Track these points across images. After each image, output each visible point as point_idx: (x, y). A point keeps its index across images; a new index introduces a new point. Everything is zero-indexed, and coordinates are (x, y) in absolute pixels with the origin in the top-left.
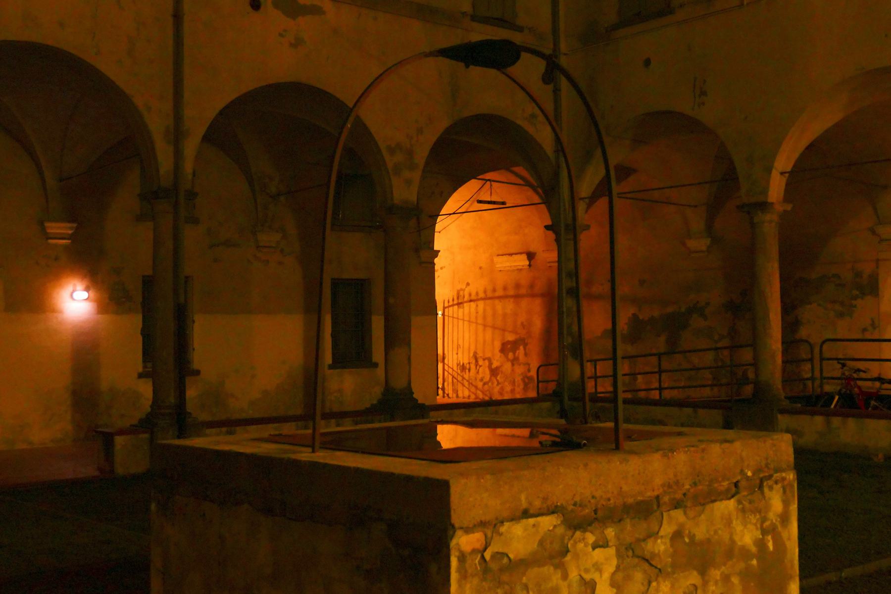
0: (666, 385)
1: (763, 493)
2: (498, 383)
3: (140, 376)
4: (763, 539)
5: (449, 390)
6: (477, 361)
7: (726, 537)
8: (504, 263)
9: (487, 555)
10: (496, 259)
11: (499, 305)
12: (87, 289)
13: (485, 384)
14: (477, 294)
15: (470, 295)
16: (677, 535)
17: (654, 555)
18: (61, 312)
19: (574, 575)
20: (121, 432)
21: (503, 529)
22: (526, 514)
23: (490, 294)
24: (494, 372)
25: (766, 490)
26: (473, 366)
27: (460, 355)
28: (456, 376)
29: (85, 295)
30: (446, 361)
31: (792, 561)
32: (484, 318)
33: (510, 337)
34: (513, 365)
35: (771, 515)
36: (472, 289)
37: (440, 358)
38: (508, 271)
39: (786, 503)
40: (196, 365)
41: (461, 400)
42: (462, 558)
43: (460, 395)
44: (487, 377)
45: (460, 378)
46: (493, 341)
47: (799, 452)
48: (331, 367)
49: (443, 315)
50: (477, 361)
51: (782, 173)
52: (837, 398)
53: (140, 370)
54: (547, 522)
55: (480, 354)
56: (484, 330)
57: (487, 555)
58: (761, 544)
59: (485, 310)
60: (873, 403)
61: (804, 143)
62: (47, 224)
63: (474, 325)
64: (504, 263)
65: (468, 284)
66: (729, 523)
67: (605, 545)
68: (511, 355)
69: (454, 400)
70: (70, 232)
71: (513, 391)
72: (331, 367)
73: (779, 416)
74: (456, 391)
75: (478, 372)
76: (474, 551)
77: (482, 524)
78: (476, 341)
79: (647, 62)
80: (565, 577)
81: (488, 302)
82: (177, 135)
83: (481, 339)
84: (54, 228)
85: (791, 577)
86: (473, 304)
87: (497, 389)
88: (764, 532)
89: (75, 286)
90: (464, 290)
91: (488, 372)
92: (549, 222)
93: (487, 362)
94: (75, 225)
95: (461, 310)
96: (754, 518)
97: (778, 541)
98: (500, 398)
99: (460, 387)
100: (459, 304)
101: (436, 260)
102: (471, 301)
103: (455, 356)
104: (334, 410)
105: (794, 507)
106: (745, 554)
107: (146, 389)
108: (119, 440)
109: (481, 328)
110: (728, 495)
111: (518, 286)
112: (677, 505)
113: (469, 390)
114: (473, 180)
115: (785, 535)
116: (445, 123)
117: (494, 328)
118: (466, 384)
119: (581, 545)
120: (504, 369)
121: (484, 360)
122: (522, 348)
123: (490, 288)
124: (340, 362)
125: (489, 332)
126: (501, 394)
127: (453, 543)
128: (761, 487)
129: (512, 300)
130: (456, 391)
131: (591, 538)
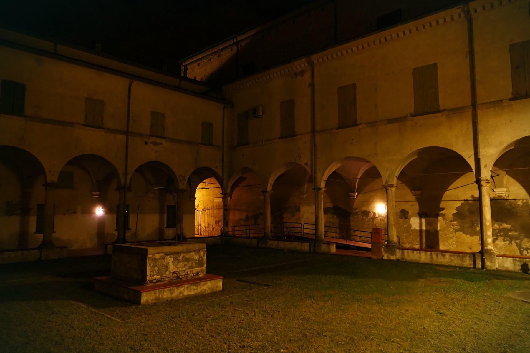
0: (251, 233)
1: (199, 252)
2: (214, 232)
3: (115, 230)
4: (199, 258)
5: (202, 233)
6: (209, 225)
7: (192, 257)
8: (216, 200)
9: (153, 258)
10: (214, 199)
11: (215, 211)
12: (103, 208)
13: (211, 232)
14: (210, 208)
15: (208, 208)
16: (183, 257)
17: (179, 259)
18: (96, 214)
19: (166, 261)
20: (109, 244)
21: (155, 255)
22: (159, 253)
23: (212, 208)
24: (213, 229)
25: (200, 252)
26: (208, 227)
27: (205, 224)
28: (204, 229)
29: (102, 210)
30: (201, 225)
31: (205, 262)
32: (211, 214)
33: (217, 220)
34: (218, 227)
35: (201, 255)
36: (208, 206)
37: (200, 225)
38: (217, 202)
39: (204, 253)
40: (130, 227)
41: (205, 236)
42: (149, 258)
43: (205, 235)
44: (212, 230)
45: (205, 230)
46: (213, 221)
47: (207, 246)
48: (166, 228)
49: (201, 213)
50: (209, 225)
51: (271, 184)
52: (286, 236)
53: (115, 228)
54: (162, 254)
55: (210, 224)
56: (211, 217)
57: (153, 258)
58: (199, 259)
59: (211, 212)
60: (293, 238)
61: (275, 178)
62: (93, 192)
63: (209, 216)
64: (216, 200)
65: (207, 205)
66: (193, 256)
67: (171, 257)
68: (217, 224)
69: (203, 236)
70: (99, 194)
71: (218, 234)
72: (166, 228)
73: (269, 241)
74: (203, 234)
75: (209, 229)
76: (151, 257)
77: (152, 254)
78: (209, 220)
79: (243, 156)
80: (164, 261)
81: (213, 210)
82: (126, 174)
83: (210, 219)
84: (94, 193)
85: (205, 264)
86: (208, 210)
87: (214, 233)
88: (200, 257)
89: (99, 207)
90: (206, 207)
91: (212, 228)
92: (221, 192)
93: (211, 226)
94: (100, 192)
95: (205, 212)
96: (198, 255)
97: (203, 259)
98: (215, 236)
99: (205, 233)
100: (205, 210)
101: (196, 200)
102: (208, 210)
103: (204, 224)
104: (213, 236)
105: (206, 254)
106: (196, 260)
107: (116, 233)
108: (109, 246)
109: (210, 217)
110: (193, 252)
111: (220, 206)
112: (183, 253)
113: (207, 234)
114: (201, 183)
115: (204, 258)
116: (193, 170)
117: (213, 217)
118: (206, 232)
119: (167, 257)
120: (216, 228)
121: (211, 225)
122: (220, 222)
123: (213, 206)
124: (168, 227)
125: (212, 218)
126: (215, 234)
127: (148, 256)
128: (199, 251)
129: (218, 210)
130: (203, 234)
131: (169, 257)
